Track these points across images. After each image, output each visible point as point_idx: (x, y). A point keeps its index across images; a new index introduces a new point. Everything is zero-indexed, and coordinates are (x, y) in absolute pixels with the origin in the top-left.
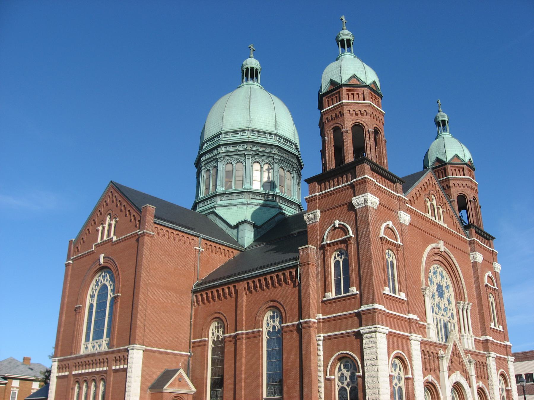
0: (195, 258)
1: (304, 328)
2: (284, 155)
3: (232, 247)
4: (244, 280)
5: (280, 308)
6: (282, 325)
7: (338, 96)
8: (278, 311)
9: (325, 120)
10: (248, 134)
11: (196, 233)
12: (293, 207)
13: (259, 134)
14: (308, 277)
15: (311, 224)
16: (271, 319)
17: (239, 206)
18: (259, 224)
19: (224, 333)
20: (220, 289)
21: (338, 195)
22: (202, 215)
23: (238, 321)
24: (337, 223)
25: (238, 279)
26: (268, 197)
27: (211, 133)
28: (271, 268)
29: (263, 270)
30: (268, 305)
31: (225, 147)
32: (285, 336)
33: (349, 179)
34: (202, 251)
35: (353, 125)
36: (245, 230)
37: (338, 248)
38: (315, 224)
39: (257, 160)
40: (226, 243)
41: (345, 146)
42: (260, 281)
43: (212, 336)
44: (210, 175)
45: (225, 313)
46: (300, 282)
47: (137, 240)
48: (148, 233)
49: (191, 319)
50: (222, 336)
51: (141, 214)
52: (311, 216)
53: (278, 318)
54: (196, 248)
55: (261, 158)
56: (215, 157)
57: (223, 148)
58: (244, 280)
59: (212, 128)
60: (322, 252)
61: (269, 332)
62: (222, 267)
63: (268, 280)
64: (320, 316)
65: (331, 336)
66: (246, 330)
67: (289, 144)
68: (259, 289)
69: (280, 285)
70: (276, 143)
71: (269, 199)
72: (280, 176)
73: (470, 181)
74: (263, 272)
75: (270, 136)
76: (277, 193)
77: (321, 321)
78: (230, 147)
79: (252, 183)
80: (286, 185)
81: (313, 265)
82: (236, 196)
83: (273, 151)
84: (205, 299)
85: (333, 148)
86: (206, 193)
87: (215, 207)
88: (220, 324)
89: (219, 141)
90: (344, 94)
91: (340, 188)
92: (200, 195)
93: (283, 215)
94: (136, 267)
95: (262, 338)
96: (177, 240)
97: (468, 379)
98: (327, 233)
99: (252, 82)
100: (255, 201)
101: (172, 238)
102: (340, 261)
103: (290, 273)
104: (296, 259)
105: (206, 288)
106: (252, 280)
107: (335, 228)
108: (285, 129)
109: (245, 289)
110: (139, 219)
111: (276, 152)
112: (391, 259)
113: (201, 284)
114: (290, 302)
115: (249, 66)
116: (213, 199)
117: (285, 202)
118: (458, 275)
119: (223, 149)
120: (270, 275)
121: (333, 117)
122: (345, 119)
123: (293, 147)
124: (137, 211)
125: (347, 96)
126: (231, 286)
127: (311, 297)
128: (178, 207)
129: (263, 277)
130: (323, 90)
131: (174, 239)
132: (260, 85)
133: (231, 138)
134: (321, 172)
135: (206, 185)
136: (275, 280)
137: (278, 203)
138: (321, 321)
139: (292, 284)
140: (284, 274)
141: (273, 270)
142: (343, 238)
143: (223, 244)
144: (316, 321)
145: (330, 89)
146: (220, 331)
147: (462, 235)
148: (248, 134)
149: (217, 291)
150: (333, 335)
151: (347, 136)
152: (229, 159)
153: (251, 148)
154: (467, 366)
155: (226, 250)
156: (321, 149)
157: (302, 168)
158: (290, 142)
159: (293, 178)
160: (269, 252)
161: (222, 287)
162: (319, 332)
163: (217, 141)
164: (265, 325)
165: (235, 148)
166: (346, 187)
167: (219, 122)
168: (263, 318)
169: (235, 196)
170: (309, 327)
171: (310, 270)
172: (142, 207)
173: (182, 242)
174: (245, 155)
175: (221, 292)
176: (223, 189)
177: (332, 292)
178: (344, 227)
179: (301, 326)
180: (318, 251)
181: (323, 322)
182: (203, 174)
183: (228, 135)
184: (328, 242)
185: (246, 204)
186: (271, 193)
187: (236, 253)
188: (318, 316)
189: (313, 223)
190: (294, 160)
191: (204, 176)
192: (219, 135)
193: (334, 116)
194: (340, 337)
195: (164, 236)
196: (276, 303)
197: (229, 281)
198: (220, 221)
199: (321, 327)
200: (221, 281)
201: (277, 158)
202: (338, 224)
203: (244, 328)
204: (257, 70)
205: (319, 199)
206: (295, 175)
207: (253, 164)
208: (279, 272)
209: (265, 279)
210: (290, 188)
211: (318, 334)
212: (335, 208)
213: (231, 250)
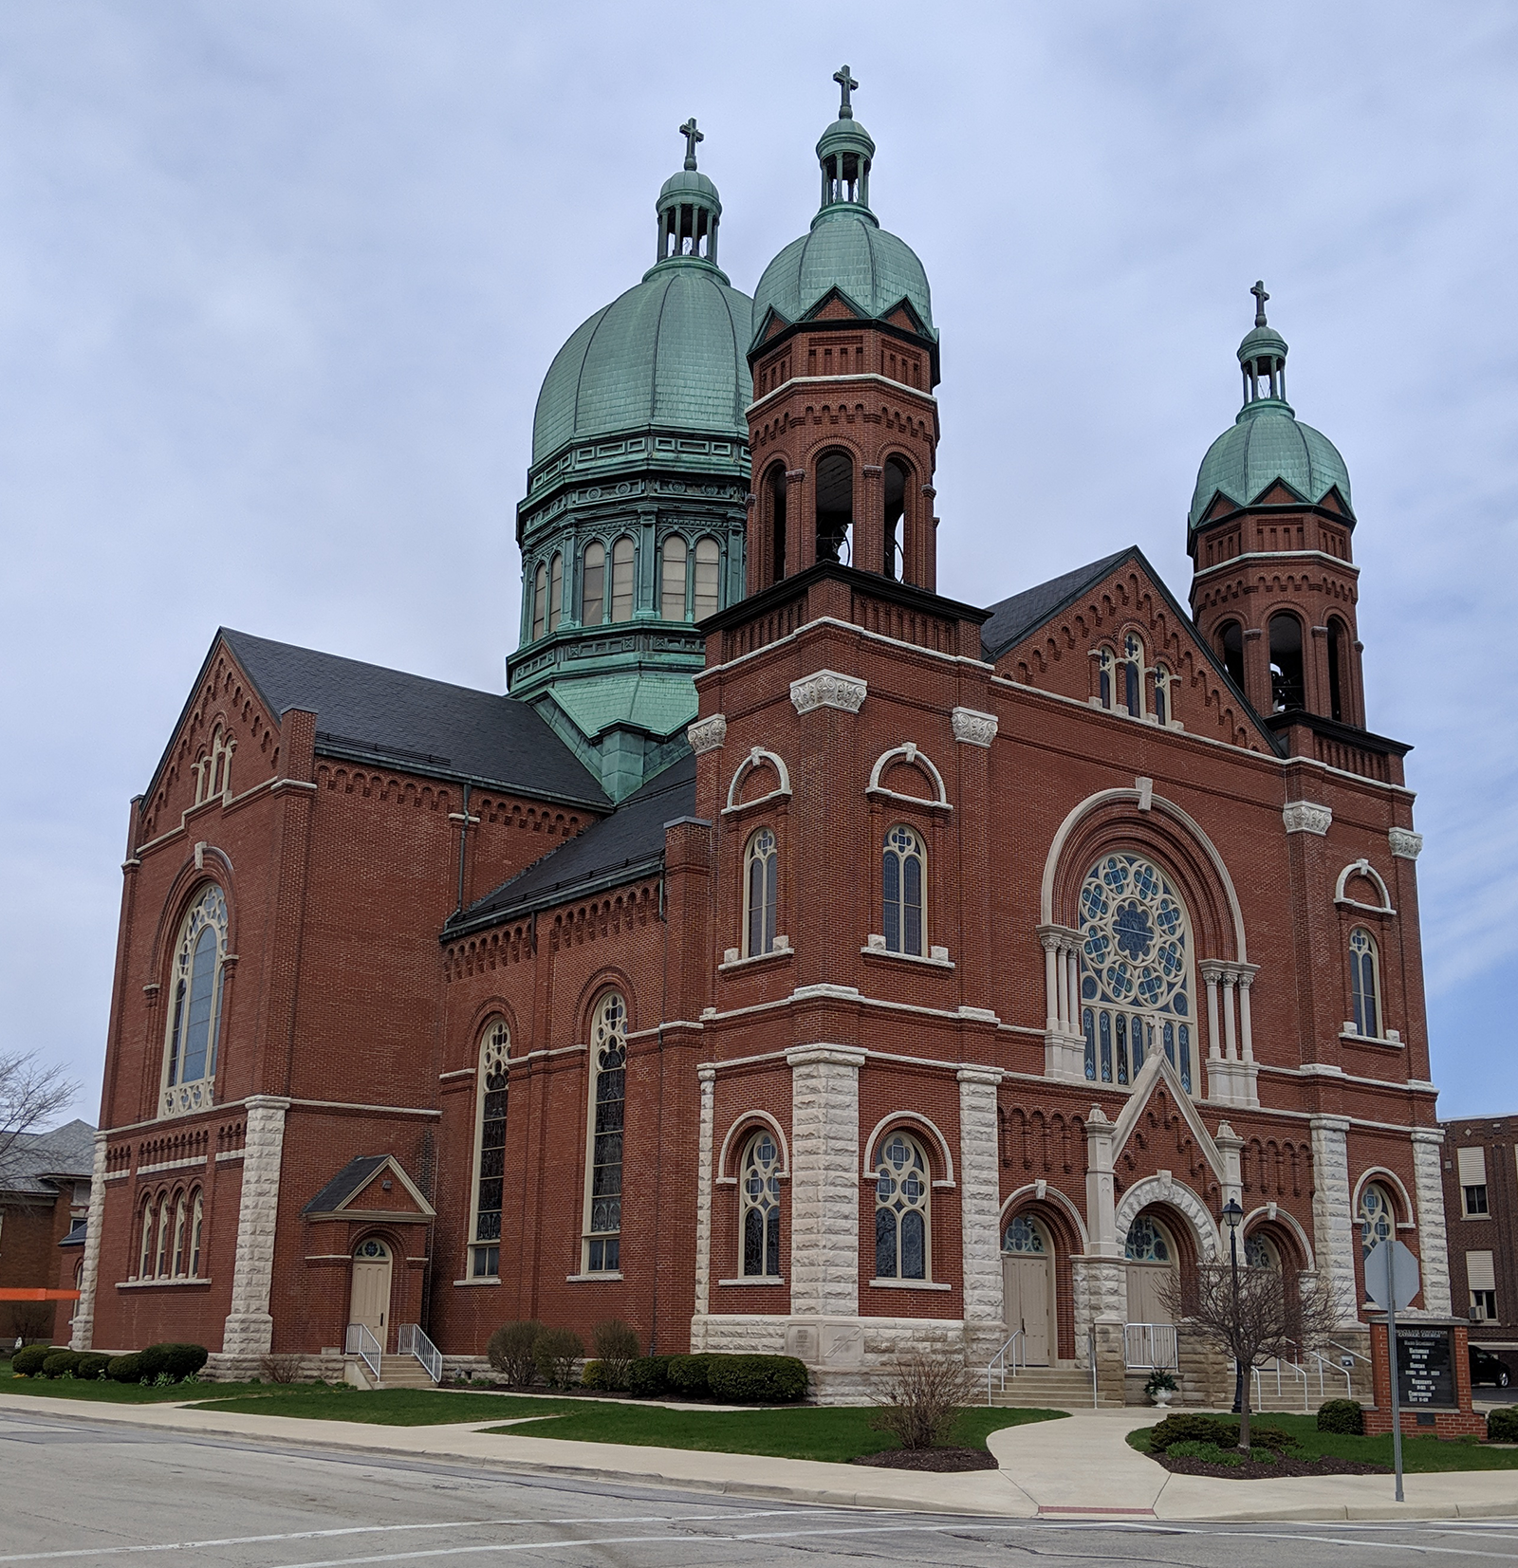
10: (646, 445)
17: (619, 677)
22: (520, 702)
39: (676, 527)
57: (575, 497)
73: (1320, 564)
75: (716, 447)
83: (725, 496)
97: (1210, 1196)
112: (910, 850)
118: (1211, 880)
133: (600, 463)
144: (701, 1026)
147: (1255, 749)
148: (646, 445)
154: (1211, 1154)
164: (483, 1061)
167: (567, 409)
207: (664, 542)
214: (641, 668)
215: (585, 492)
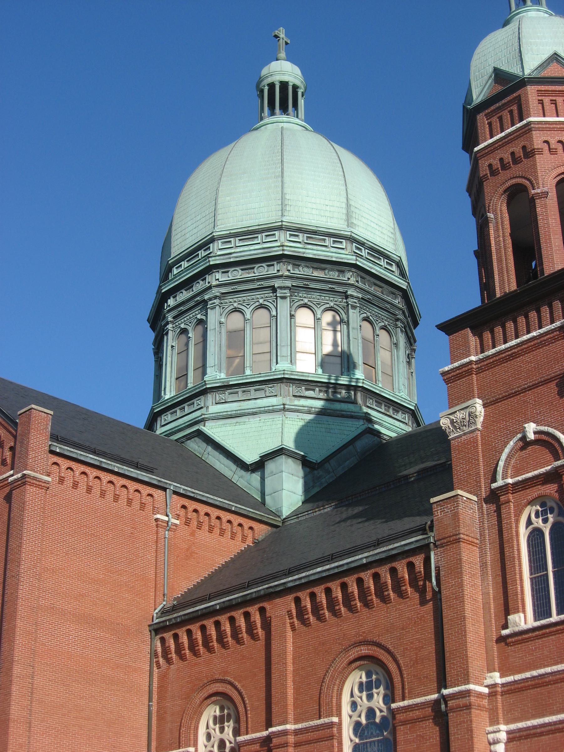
0: (157, 542)
1: (453, 709)
2: (372, 289)
3: (251, 515)
4: (286, 591)
5: (385, 661)
6: (393, 706)
7: (515, 108)
8: (379, 670)
9: (484, 169)
11: (159, 479)
12: (400, 416)
13: (308, 237)
14: (460, 574)
15: (460, 436)
16: (361, 691)
17: (263, 417)
18: (316, 457)
19: (237, 732)
20: (223, 619)
21: (527, 357)
22: (172, 440)
23: (274, 700)
24: (531, 429)
25: (272, 590)
26: (335, 392)
27: (188, 241)
28: (357, 557)
29: (336, 564)
30: (354, 653)
31: (223, 272)
32: (402, 734)
33: (555, 315)
34: (176, 525)
35: (559, 178)
36: (282, 472)
37: (535, 495)
38: (471, 435)
39: (306, 301)
40: (234, 506)
41: (542, 231)
42: (328, 591)
43: (206, 743)
44: (187, 344)
45: (239, 682)
46: (437, 589)
47: (8, 498)
48: (35, 478)
49: (150, 700)
50: (233, 741)
51: (16, 431)
52: (459, 415)
53: (381, 690)
54: (158, 516)
55: (316, 295)
56: (198, 298)
58: (286, 591)
59: (189, 229)
60: (493, 507)
61: (358, 725)
62: (226, 566)
63: (350, 590)
64: (496, 678)
65: (528, 728)
66: (295, 723)
67: (383, 262)
68: (327, 613)
69: (385, 599)
70: (352, 259)
71: (339, 396)
72: (364, 339)
74: (337, 567)
76: (357, 382)
77: (499, 689)
78: (235, 272)
79: (296, 359)
80: (379, 363)
81: (471, 543)
82: (256, 390)
84: (186, 645)
85: (509, 241)
86: (178, 389)
87: (202, 421)
88: (226, 711)
89: (208, 257)
90: (531, 103)
91: (534, 338)
92: (165, 394)
93: (375, 435)
94: (6, 565)
95: (340, 743)
96: (110, 496)
98: (504, 456)
99: (284, 118)
100: (303, 402)
101: (96, 491)
102: (544, 529)
103: (411, 566)
104: (425, 530)
105: (187, 617)
106: (309, 591)
107: (525, 443)
108: (373, 225)
109: (291, 616)
110: (12, 444)
111: (352, 281)
113: (174, 609)
114: (412, 643)
115: (277, 79)
116: (200, 401)
117: (379, 404)
119: (219, 277)
120: (356, 576)
121: (506, 161)
122: (538, 164)
123: (394, 268)
124: (6, 425)
125: (540, 107)
126: (254, 610)
127: (470, 627)
128: (109, 420)
129: (338, 582)
130: (474, 97)
131: (103, 494)
132: (304, 124)
134: (479, 304)
135: (179, 370)
136: (369, 587)
137: (361, 407)
138: (499, 689)
139: (417, 595)
140: (393, 571)
141: (364, 561)
142: (549, 467)
143: (226, 506)
144: (486, 690)
145: (495, 92)
146: (226, 728)
149: (217, 624)
150: (534, 727)
151: (545, 206)
152: (234, 302)
153: (289, 270)
155: (235, 524)
156: (476, 248)
157: (416, 324)
158: (386, 257)
159: (396, 345)
160: (349, 522)
161: (229, 615)
162: (494, 721)
163: (202, 258)
164: (346, 709)
165: (249, 273)
166: (552, 335)
168: (342, 689)
169: (253, 392)
170: (468, 707)
171: (465, 557)
172: (19, 413)
173: (123, 501)
174: (274, 289)
175: (227, 627)
176: (223, 376)
177: (524, 612)
178: (550, 440)
179: (446, 706)
180: (482, 506)
181: (503, 693)
182: (171, 340)
183: (230, 242)
184: (510, 481)
185: (280, 410)
186: (344, 380)
187: (261, 531)
188: (491, 677)
189: (465, 434)
190: (398, 301)
191: (172, 346)
192: (205, 244)
193: (508, 158)
194: (553, 732)
195: (75, 485)
196: (375, 648)
197: (248, 598)
198: (216, 454)
199: (500, 705)
200: (227, 599)
201: (355, 294)
202: (535, 433)
203: (291, 717)
204: (295, 88)
205: (479, 371)
206: (402, 339)
207: (295, 312)
208: (380, 565)
209: (344, 586)
210: (390, 369)
211: (491, 724)
212: (525, 390)
213: (247, 523)
214: (284, 410)
215: (228, 272)
